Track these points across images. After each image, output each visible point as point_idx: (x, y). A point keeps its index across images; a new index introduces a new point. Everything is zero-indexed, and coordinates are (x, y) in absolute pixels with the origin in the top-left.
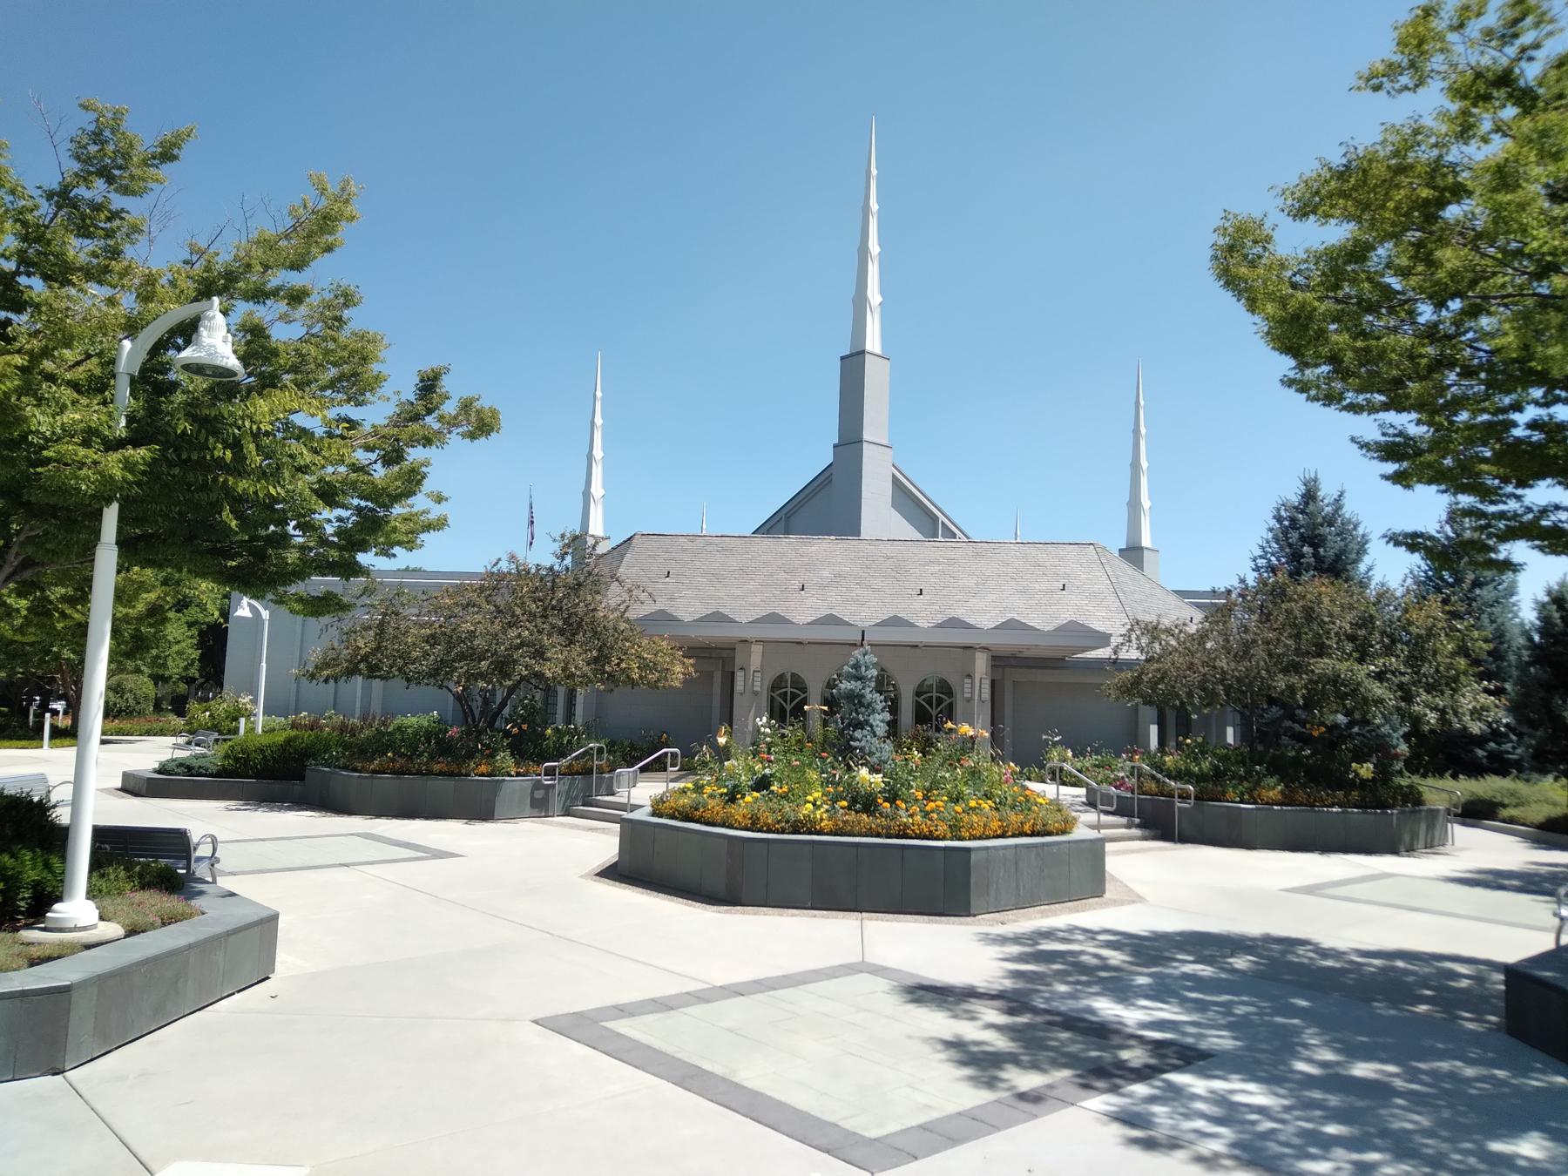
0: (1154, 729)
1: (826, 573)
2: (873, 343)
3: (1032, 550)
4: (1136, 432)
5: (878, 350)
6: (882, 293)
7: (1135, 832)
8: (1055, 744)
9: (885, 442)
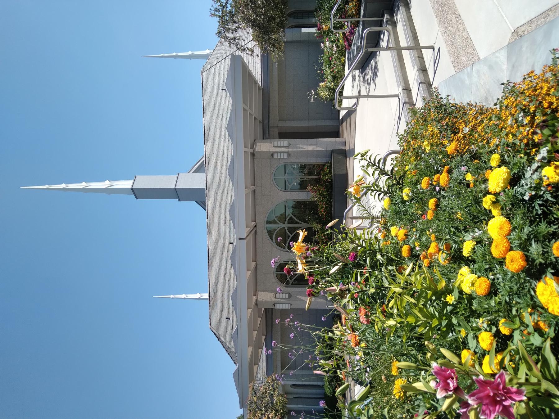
0: (304, 30)
1: (224, 228)
2: (127, 184)
3: (207, 108)
4: (175, 57)
5: (131, 182)
6: (104, 180)
7: (400, 16)
8: (316, 94)
9: (176, 176)
